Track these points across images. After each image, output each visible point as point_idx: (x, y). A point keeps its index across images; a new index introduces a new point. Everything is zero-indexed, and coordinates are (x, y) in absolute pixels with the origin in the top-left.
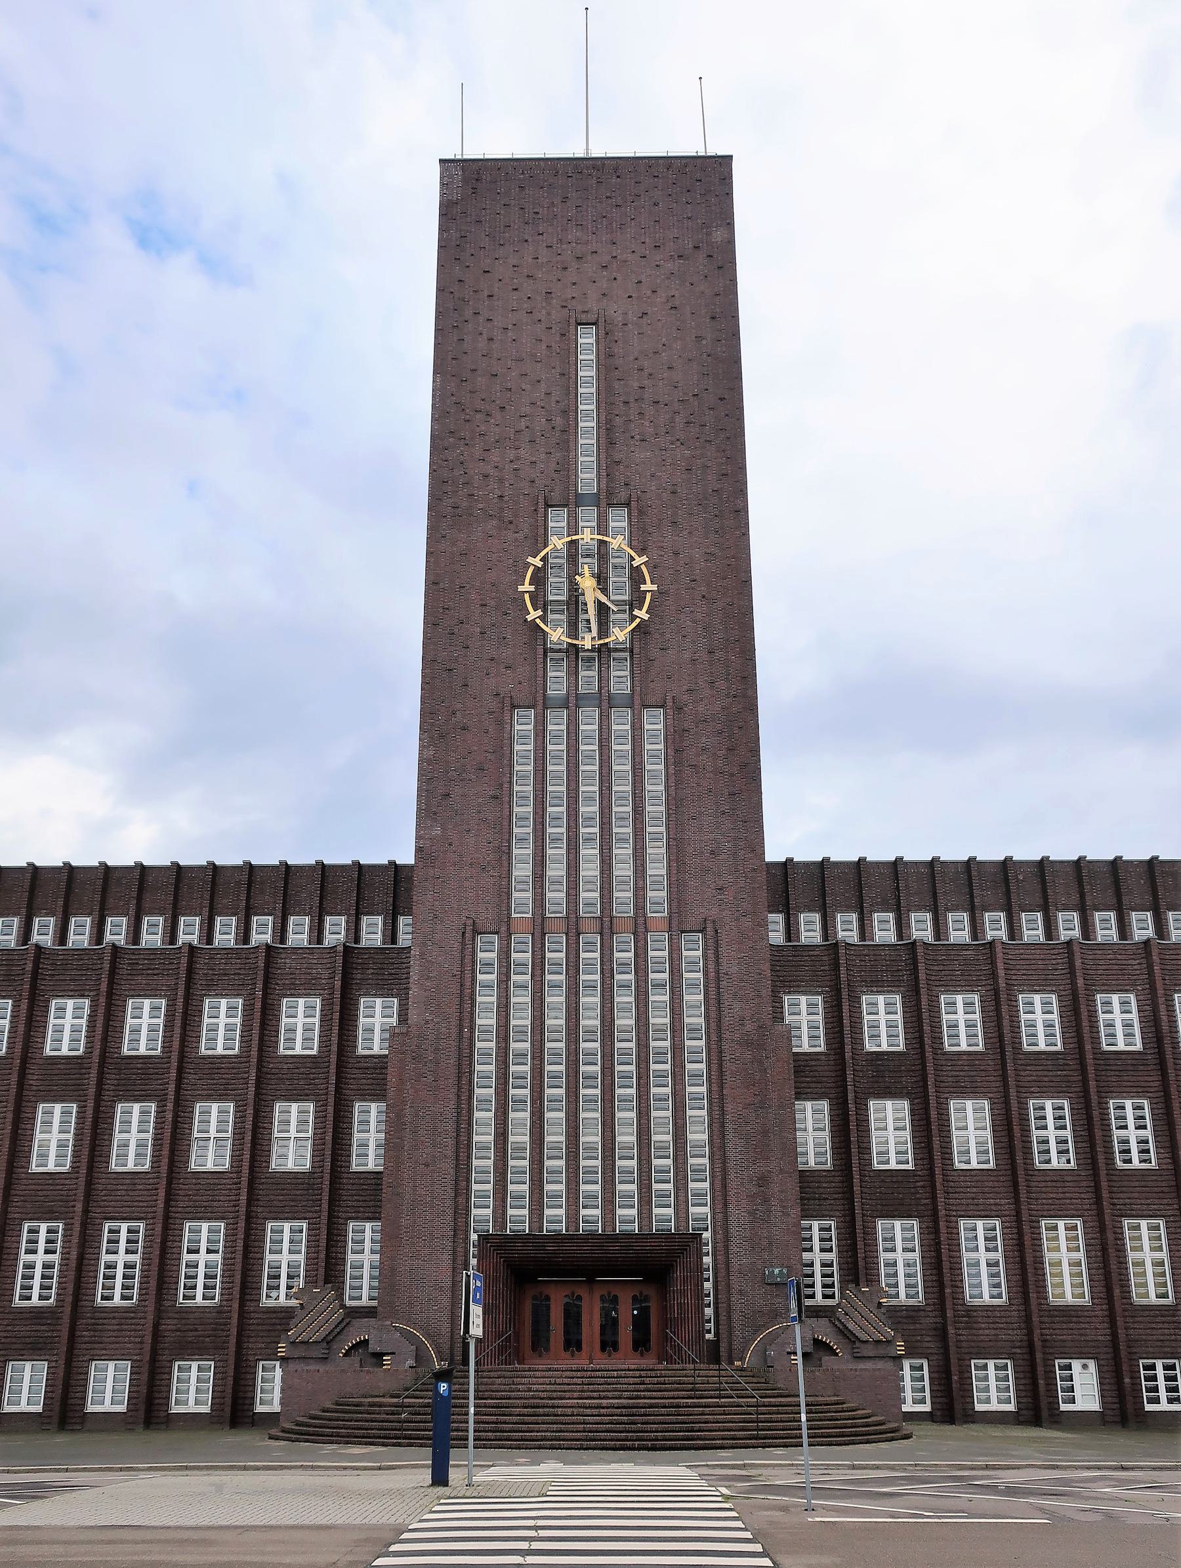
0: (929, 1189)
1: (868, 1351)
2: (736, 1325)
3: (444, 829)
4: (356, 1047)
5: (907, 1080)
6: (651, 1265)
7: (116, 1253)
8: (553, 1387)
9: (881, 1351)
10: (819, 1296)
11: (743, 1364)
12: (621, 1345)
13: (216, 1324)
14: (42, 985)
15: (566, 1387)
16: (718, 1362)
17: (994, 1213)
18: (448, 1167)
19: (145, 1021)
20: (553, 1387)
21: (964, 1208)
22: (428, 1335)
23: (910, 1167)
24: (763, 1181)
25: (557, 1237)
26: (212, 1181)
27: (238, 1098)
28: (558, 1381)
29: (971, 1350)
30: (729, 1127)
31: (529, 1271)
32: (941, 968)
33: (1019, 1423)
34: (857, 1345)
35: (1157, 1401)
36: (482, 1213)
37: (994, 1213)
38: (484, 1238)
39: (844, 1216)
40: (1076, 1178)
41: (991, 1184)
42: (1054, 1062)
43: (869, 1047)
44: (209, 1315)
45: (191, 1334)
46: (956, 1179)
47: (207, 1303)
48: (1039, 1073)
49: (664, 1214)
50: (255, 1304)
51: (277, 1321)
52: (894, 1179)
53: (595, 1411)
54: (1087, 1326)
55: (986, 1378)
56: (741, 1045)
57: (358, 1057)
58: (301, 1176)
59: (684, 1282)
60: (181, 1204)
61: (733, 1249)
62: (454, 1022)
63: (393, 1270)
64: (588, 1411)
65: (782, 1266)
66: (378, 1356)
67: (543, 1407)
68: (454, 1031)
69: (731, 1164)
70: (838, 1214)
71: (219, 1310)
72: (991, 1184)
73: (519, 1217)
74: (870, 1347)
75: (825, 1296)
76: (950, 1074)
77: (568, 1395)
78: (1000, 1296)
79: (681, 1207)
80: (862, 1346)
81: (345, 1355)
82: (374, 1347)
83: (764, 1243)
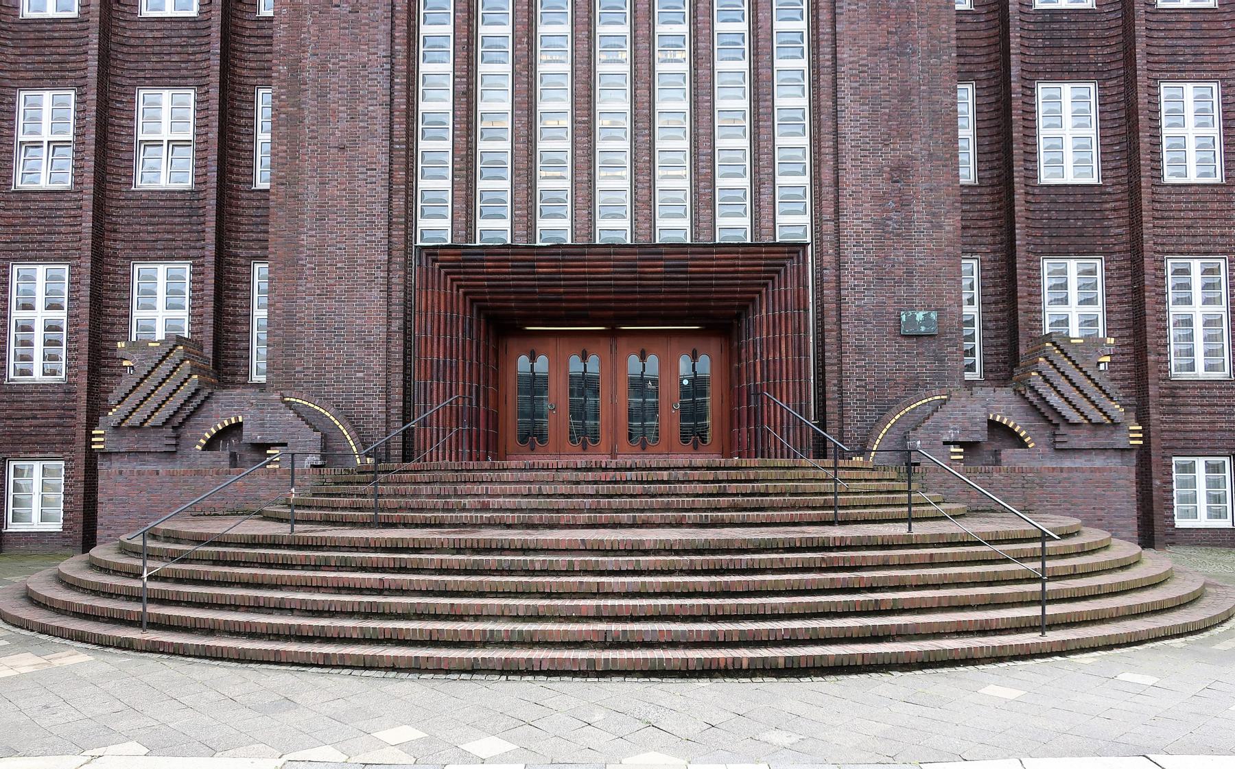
2: (851, 401)
6: (708, 297)
8: (534, 502)
9: (1102, 439)
15: (562, 503)
17: (1219, 249)
18: (376, 151)
20: (534, 502)
21: (1174, 240)
22: (349, 419)
24: (900, 172)
25: (557, 251)
28: (547, 489)
29: (1174, 443)
30: (845, 85)
31: (508, 310)
34: (1063, 429)
37: (1219, 249)
38: (432, 252)
41: (1216, 206)
44: (52, 397)
46: (1165, 198)
47: (50, 379)
49: (733, 225)
52: (1071, 199)
53: (624, 561)
57: (259, 20)
58: (179, 196)
61: (848, 280)
63: (290, 315)
64: (610, 561)
65: (928, 308)
67: (501, 550)
69: (846, 146)
70: (984, 249)
71: (67, 390)
73: (495, 227)
74: (1084, 433)
76: (1163, 43)
77: (566, 517)
80: (1071, 432)
82: (251, 434)
83: (900, 272)
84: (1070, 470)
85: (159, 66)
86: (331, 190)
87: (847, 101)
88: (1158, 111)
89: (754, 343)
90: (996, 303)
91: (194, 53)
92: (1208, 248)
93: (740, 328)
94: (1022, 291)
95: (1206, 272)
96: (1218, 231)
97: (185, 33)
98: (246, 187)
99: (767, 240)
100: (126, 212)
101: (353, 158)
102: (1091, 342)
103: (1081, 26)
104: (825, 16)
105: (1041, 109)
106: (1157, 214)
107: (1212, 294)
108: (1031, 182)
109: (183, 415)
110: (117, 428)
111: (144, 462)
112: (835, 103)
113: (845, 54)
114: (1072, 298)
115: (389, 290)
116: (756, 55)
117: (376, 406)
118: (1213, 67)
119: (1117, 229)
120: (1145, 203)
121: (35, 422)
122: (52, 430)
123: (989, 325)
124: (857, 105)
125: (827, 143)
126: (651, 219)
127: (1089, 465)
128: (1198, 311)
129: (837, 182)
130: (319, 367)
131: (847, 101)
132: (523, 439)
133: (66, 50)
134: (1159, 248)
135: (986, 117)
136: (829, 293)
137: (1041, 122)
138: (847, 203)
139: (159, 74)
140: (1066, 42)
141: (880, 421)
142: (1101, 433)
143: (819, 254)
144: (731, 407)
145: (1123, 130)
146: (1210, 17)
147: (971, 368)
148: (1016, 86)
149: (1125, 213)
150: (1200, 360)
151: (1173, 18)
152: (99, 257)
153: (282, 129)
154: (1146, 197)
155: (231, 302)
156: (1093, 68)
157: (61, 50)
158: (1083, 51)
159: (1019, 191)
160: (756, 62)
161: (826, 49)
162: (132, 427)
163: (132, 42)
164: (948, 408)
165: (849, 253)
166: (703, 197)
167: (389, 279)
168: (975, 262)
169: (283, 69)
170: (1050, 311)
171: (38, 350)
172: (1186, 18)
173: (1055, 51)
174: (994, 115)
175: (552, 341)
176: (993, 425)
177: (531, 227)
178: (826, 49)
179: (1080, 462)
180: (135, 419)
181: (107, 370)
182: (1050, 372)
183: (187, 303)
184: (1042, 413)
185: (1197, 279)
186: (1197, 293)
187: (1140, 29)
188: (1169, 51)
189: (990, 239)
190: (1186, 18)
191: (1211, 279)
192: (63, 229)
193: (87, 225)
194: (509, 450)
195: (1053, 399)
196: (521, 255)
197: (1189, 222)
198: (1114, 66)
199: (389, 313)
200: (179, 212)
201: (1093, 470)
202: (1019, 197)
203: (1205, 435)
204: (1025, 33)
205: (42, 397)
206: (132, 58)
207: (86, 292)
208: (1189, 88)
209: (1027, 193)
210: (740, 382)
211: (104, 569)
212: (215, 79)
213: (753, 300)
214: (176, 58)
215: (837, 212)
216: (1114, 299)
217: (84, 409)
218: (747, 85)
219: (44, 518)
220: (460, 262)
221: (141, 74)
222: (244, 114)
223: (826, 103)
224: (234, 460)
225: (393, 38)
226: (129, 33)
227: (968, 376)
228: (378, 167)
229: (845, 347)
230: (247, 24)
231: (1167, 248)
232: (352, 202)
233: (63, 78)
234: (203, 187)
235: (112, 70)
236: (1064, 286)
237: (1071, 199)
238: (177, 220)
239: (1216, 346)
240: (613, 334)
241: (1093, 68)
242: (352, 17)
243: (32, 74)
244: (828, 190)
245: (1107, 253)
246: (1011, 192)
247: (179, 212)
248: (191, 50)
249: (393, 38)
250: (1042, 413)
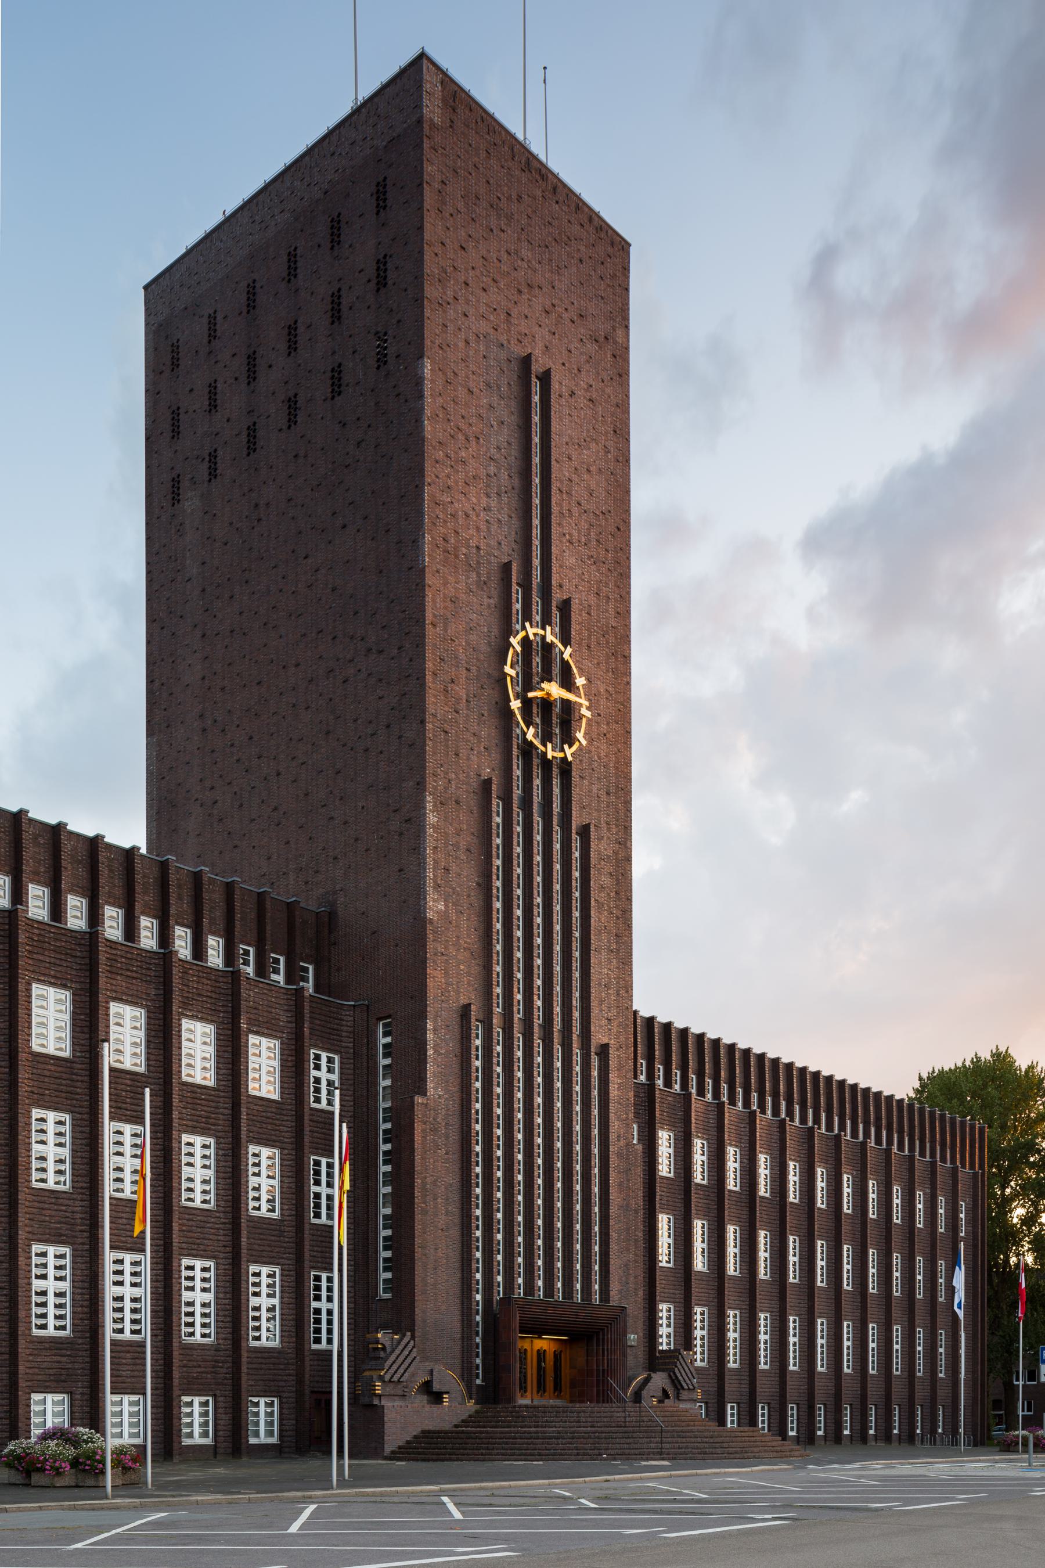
3: (446, 906)
10: (127, 1331)
13: (216, 1361)
27: (220, 1134)
44: (209, 1353)
45: (195, 1370)
51: (263, 1361)
71: (215, 1348)
75: (133, 1332)
78: (63, 1328)
85: (261, 1130)
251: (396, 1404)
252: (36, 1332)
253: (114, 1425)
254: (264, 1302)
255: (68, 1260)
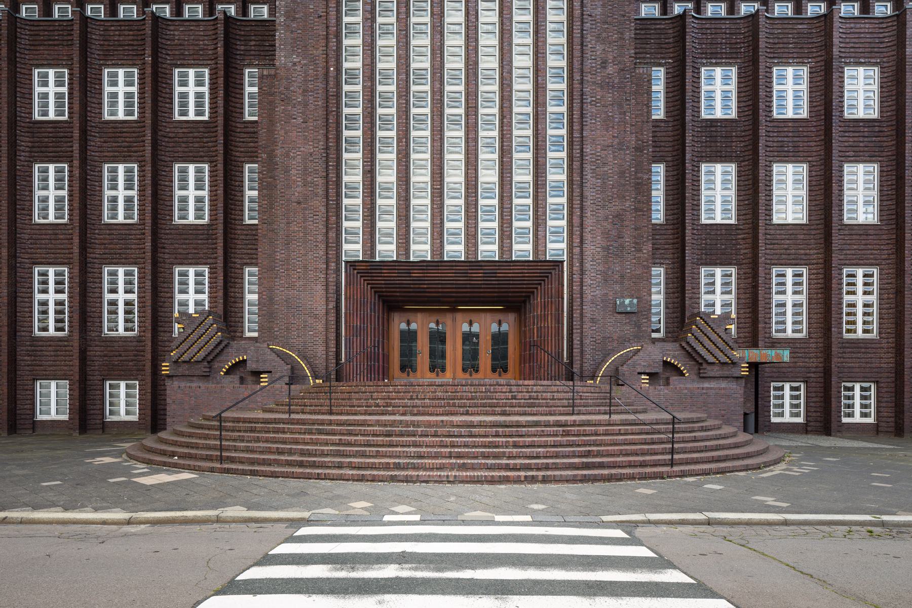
0: (750, 244)
1: (715, 371)
2: (588, 350)
4: (242, 113)
5: (738, 146)
6: (512, 289)
7: (47, 292)
11: (595, 382)
12: (481, 368)
14: (92, 154)
16: (572, 380)
17: (803, 262)
18: (318, 204)
19: (52, 89)
23: (733, 222)
26: (123, 232)
29: (774, 374)
30: (588, 167)
32: (776, 41)
33: (807, 432)
34: (705, 366)
35: (781, 415)
36: (353, 249)
37: (803, 262)
38: (352, 265)
39: (673, 263)
40: (877, 232)
41: (802, 237)
42: (870, 129)
43: (704, 115)
44: (130, 344)
45: (116, 359)
48: (856, 139)
49: (522, 249)
50: (169, 334)
54: (872, 355)
55: (782, 397)
56: (602, 87)
57: (245, 122)
58: (201, 228)
59: (545, 307)
60: (96, 252)
61: (587, 281)
62: (321, 63)
63: (271, 299)
65: (632, 297)
66: (257, 374)
68: (321, 71)
69: (588, 203)
71: (139, 339)
72: (802, 237)
73: (387, 250)
74: (716, 368)
79: (539, 241)
80: (709, 368)
81: (226, 373)
82: (251, 366)
84: (707, 388)
85: (186, 150)
86: (294, 227)
87: (588, 177)
88: (771, 181)
89: (534, 317)
90: (673, 293)
91: (207, 142)
92: (796, 262)
93: (525, 308)
94: (688, 287)
95: (795, 275)
96: (802, 252)
97: (201, 130)
98: (240, 222)
99: (542, 258)
100: (170, 236)
101: (305, 209)
102: (725, 317)
103: (729, 129)
104: (576, 127)
105: (703, 178)
106: (767, 241)
107: (798, 288)
108: (695, 222)
109: (213, 355)
110: (176, 362)
111: (192, 381)
112: (582, 178)
113: (588, 149)
114: (717, 291)
115: (327, 285)
116: (537, 149)
117: (320, 350)
118: (805, 154)
119: (744, 250)
120: (761, 236)
121: (121, 358)
122: (131, 363)
123: (670, 306)
124: (594, 180)
125: (577, 202)
126: (476, 245)
127: (717, 386)
128: (789, 298)
129: (582, 225)
130: (288, 329)
131: (588, 177)
132: (403, 368)
133: (131, 140)
134: (769, 262)
135: (671, 183)
136: (576, 288)
137: (703, 186)
138: (588, 236)
139: (187, 154)
140: (719, 139)
141: (604, 361)
142: (725, 368)
143: (571, 266)
144: (520, 352)
145: (750, 192)
146: (804, 124)
147: (658, 331)
148: (688, 165)
149: (749, 241)
150: (789, 327)
151: (782, 124)
152: (155, 263)
153: (265, 191)
154: (761, 231)
155: (233, 290)
156: (734, 154)
157: (127, 139)
158: (729, 144)
159: (689, 227)
160: (537, 154)
161: (577, 147)
162: (184, 362)
163: (170, 135)
164: (641, 353)
165: (588, 265)
166: (505, 234)
167: (327, 278)
168: (662, 269)
169: (264, 156)
170: (705, 298)
171: (789, 319)
172: (790, 124)
173: (713, 144)
174: (675, 182)
175: (483, 315)
176: (666, 363)
177: (407, 250)
178: (577, 147)
179: (713, 384)
180: (186, 357)
181: (162, 329)
182: (699, 334)
183: (207, 290)
184: (692, 355)
185: (789, 279)
186: (789, 288)
187: (762, 132)
188: (780, 144)
189: (671, 256)
190: (790, 124)
191: (798, 279)
192: (133, 246)
193: (148, 244)
194: (396, 376)
195: (699, 348)
196: (404, 265)
197: (786, 246)
198: (747, 153)
199: (327, 298)
200: (201, 237)
201: (720, 389)
202: (688, 232)
203: (790, 370)
204: (695, 134)
205: (124, 344)
206: (171, 145)
207: (148, 284)
208: (790, 167)
209: (693, 229)
210: (525, 338)
211: (165, 442)
212: (220, 158)
213: (533, 292)
214: (197, 145)
215: (582, 242)
216: (742, 291)
217: (150, 351)
218: (531, 167)
219: (128, 413)
220: (367, 269)
221: (176, 155)
222: (238, 179)
223: (577, 178)
224: (242, 380)
225: (327, 139)
226: (168, 130)
227: (654, 335)
228: (320, 214)
229: (585, 319)
230: (238, 125)
231: (773, 262)
232: (305, 234)
233: (130, 156)
234: (215, 222)
235: (160, 153)
236: (713, 283)
237: (719, 232)
238: (200, 242)
239: (799, 318)
240: (454, 310)
241: (734, 154)
242: (304, 125)
243: (112, 154)
244: (576, 230)
245: (738, 264)
246: (684, 228)
247: (201, 237)
248: (205, 140)
249: (327, 139)
250: (692, 355)
251: (194, 385)
252: (846, 336)
253: (776, 406)
254: (121, 297)
255: (804, 278)
